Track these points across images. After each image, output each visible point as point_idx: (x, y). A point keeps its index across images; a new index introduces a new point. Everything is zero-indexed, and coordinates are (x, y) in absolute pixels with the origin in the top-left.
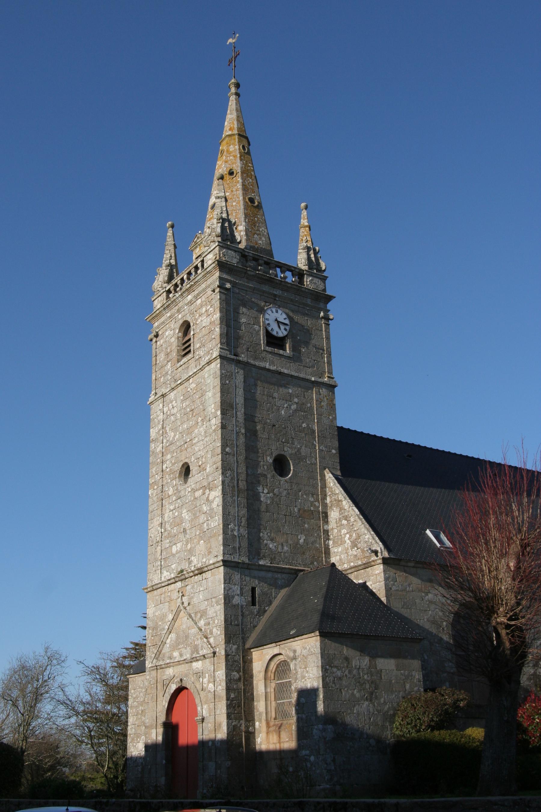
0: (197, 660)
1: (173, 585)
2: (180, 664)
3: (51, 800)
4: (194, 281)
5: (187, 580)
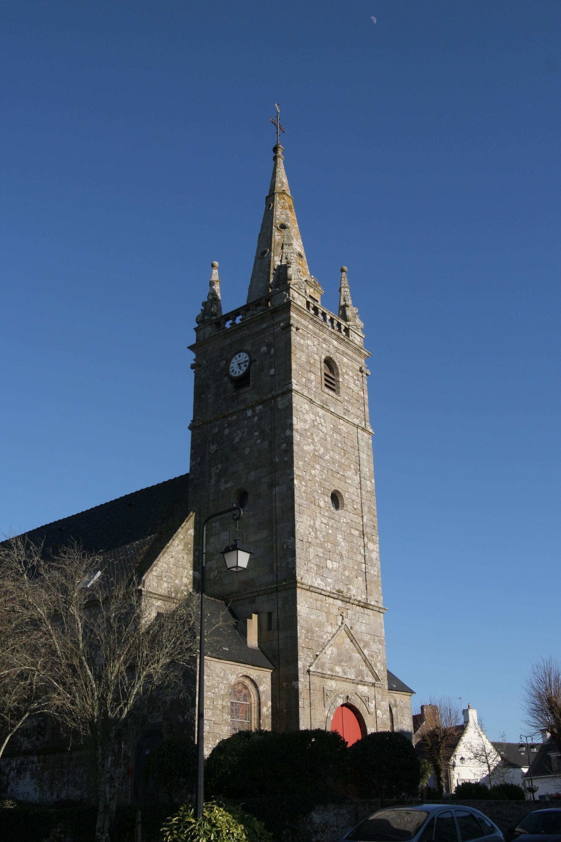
0: (364, 685)
1: (332, 599)
2: (345, 681)
3: (436, 801)
4: (348, 341)
5: (348, 604)
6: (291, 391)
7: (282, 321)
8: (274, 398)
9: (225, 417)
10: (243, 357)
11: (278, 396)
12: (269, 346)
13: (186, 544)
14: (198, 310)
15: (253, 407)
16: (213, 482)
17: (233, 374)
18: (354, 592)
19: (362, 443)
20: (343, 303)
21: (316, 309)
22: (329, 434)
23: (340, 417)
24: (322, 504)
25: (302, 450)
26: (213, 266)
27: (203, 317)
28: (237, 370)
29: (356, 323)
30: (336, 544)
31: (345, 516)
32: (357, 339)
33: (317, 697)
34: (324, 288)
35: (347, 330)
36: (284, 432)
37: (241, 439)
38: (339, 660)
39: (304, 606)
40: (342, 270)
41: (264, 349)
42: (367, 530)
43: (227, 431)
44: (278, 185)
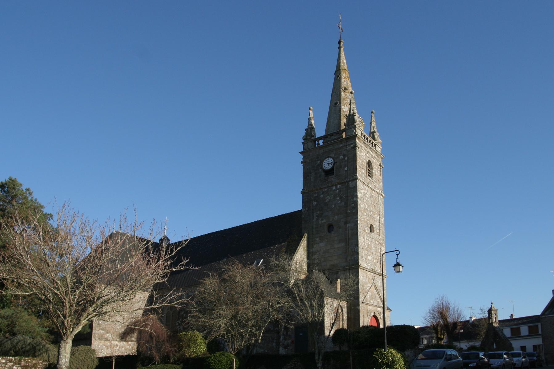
6: (356, 179)
7: (352, 144)
8: (348, 182)
9: (321, 189)
10: (330, 160)
11: (350, 181)
12: (344, 156)
13: (304, 248)
14: (303, 133)
15: (336, 186)
16: (315, 219)
17: (325, 168)
18: (377, 269)
19: (380, 201)
20: (372, 130)
21: (364, 136)
22: (370, 198)
23: (373, 190)
24: (367, 231)
25: (361, 207)
26: (310, 109)
27: (306, 137)
28: (327, 166)
29: (379, 141)
30: (371, 249)
31: (374, 236)
32: (379, 149)
33: (365, 312)
34: (365, 124)
35: (375, 145)
36: (353, 199)
37: (330, 200)
38: (373, 297)
39: (362, 275)
40: (372, 113)
41: (341, 157)
42: (381, 242)
43: (322, 196)
44: (342, 64)
